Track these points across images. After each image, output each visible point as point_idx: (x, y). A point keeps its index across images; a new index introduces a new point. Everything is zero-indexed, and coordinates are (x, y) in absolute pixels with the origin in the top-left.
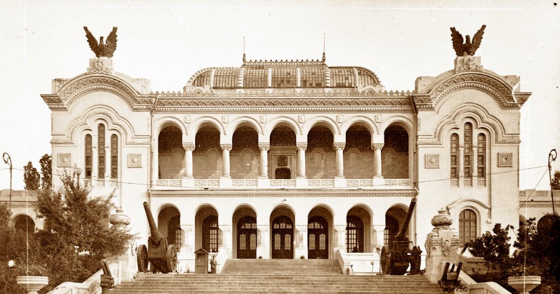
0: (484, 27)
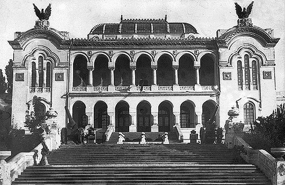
0: (253, 2)
